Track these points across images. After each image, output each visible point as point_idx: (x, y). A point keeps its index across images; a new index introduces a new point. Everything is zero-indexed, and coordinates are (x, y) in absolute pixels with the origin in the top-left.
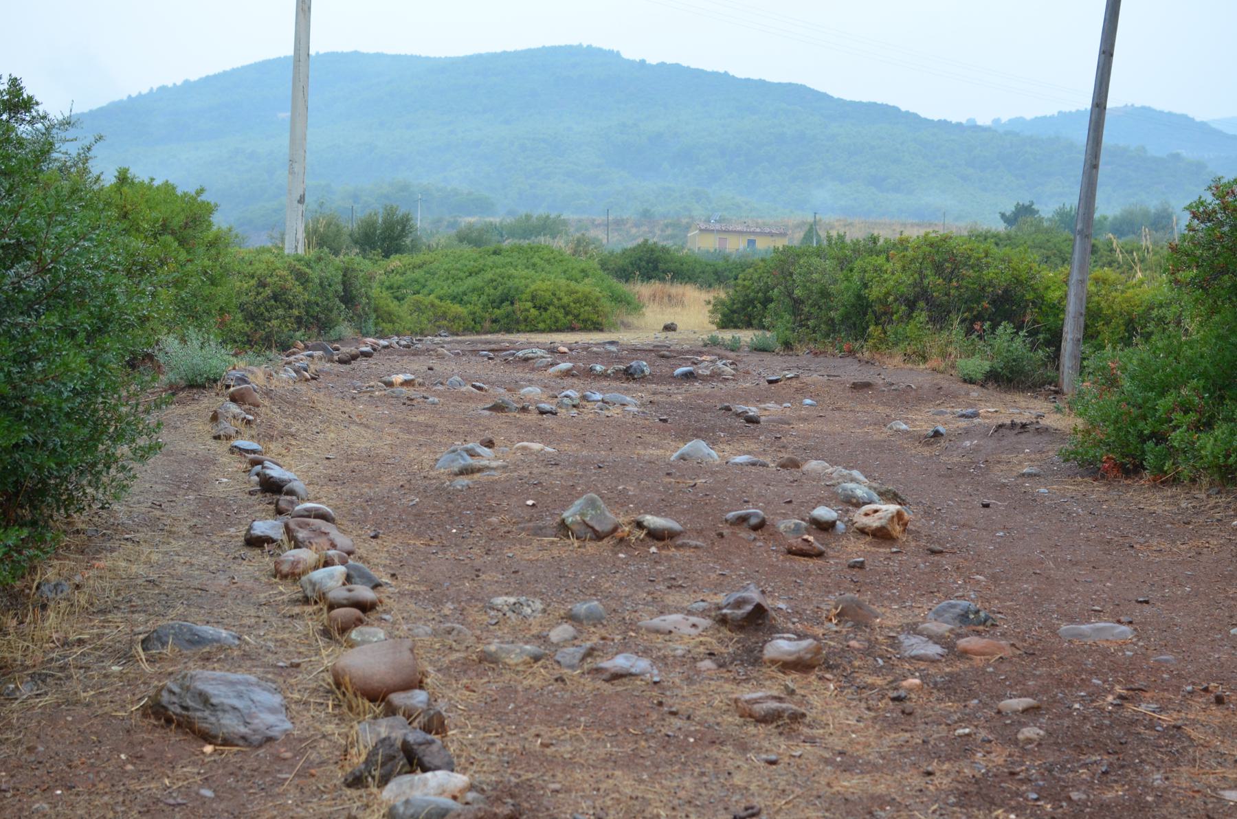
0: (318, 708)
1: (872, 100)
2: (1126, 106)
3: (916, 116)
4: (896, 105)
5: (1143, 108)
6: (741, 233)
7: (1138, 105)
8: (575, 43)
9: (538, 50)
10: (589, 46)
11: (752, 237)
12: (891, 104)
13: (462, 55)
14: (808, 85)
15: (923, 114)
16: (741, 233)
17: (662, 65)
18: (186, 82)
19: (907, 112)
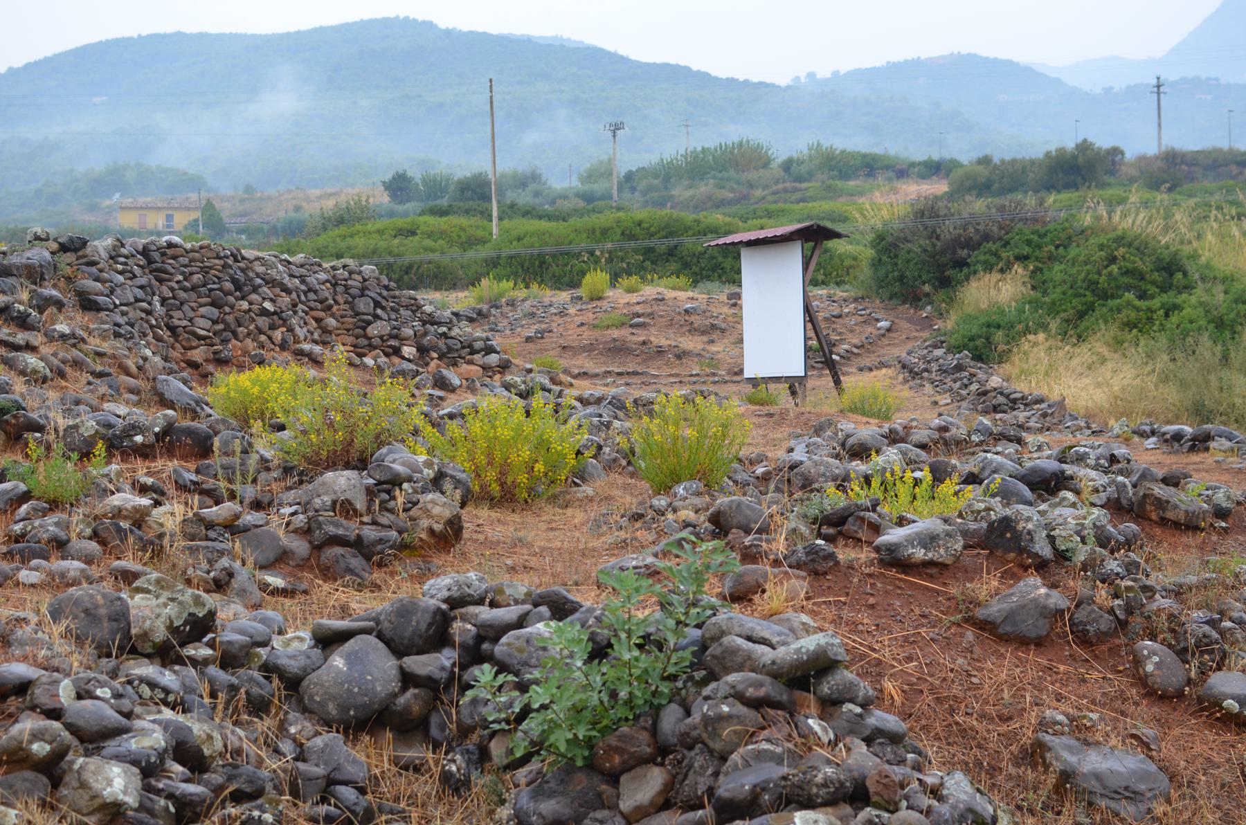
0: (727, 228)
1: (666, 61)
2: (952, 54)
3: (706, 75)
4: (688, 65)
5: (969, 55)
6: (160, 209)
7: (964, 52)
8: (392, 15)
9: (355, 23)
10: (406, 18)
11: (170, 212)
12: (682, 63)
13: (263, 33)
14: (984, 52)
15: (714, 73)
16: (160, 209)
17: (471, 33)
18: (10, 70)
19: (699, 72)
